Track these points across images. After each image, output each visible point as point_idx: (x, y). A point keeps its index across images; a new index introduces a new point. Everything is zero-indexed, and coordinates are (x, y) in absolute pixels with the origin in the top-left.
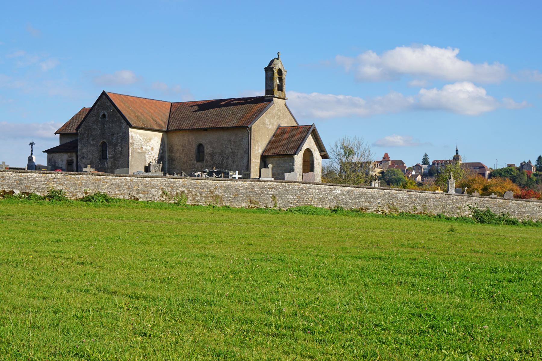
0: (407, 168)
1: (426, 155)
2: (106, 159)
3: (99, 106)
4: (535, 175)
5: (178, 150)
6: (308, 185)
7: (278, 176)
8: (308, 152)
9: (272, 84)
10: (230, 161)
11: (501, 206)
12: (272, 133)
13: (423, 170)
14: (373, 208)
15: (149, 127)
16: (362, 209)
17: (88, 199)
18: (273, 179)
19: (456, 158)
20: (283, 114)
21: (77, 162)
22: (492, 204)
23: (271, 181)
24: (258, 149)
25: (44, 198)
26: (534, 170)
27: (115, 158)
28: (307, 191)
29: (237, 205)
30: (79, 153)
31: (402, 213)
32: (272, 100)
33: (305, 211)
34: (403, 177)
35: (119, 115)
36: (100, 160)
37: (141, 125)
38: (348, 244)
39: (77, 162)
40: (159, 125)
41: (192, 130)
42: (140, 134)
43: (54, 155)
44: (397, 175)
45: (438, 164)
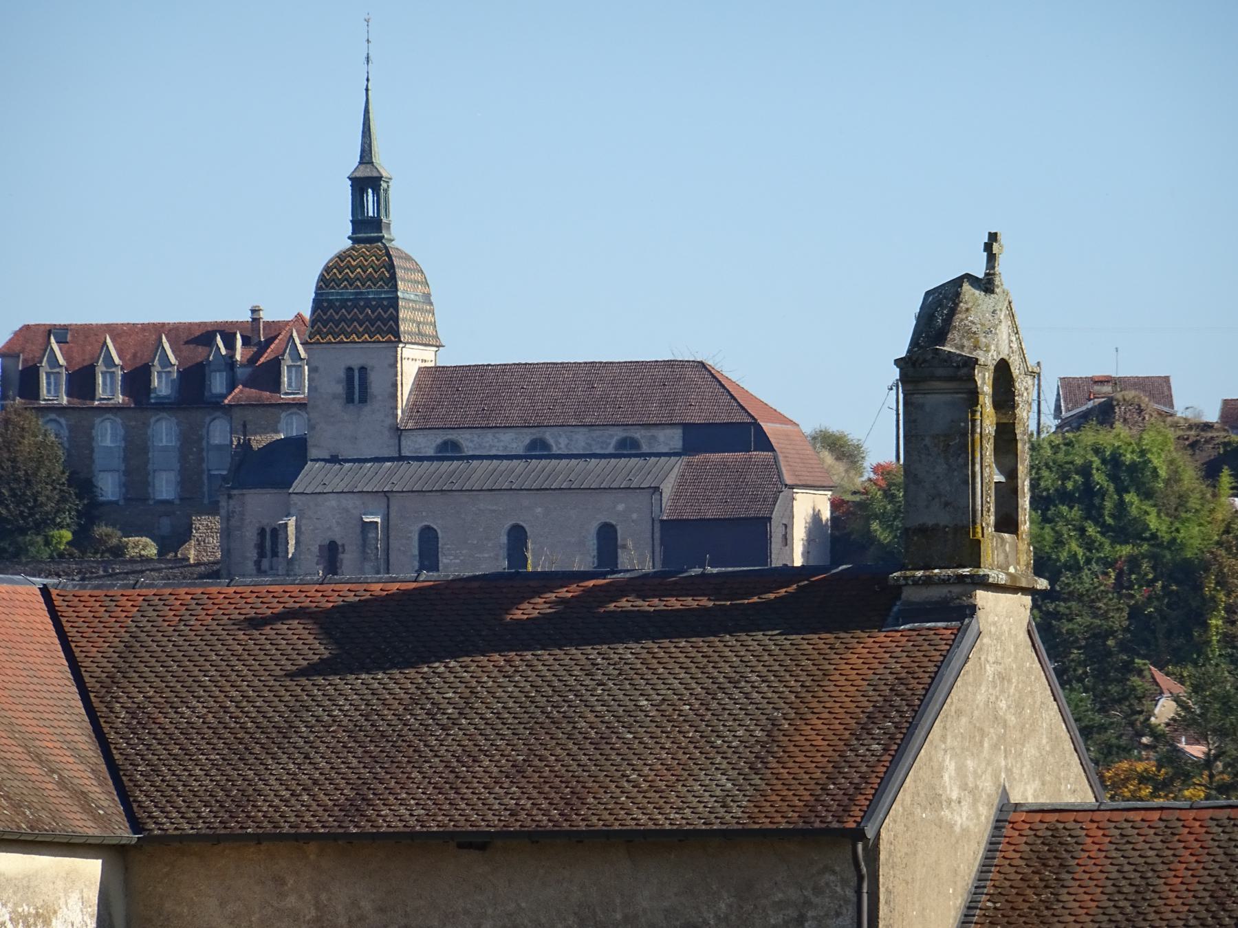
12: (967, 859)
19: (362, 296)
20: (1019, 707)
32: (973, 610)
45: (82, 381)
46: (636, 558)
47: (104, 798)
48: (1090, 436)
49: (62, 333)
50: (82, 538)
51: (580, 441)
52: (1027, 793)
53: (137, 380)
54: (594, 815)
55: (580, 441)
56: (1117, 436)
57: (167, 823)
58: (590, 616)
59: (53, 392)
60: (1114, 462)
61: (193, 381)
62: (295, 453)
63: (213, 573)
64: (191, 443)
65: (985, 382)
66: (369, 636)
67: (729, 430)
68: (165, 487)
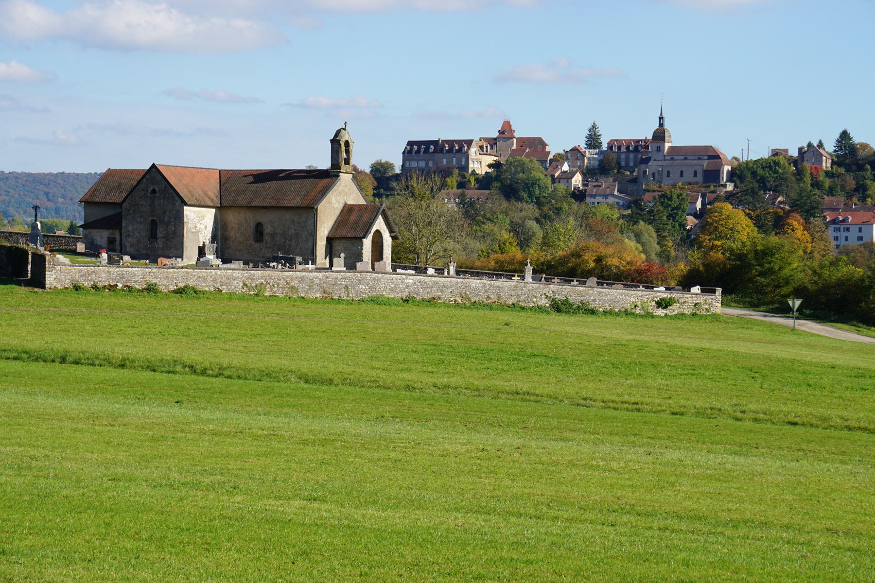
0: (551, 157)
1: (594, 127)
4: (828, 174)
5: (232, 228)
6: (380, 275)
7: (351, 266)
8: (378, 233)
9: (339, 158)
11: (580, 295)
12: (337, 212)
13: (586, 160)
14: (445, 297)
15: (203, 203)
16: (434, 299)
17: (180, 291)
19: (660, 135)
22: (573, 292)
23: (344, 272)
24: (323, 231)
25: (142, 290)
26: (826, 164)
27: (167, 238)
28: (379, 280)
29: (312, 296)
30: (123, 231)
31: (475, 302)
33: (377, 301)
34: (542, 177)
35: (172, 191)
37: (195, 202)
38: (419, 337)
40: (212, 200)
41: (249, 208)
42: (194, 212)
43: (91, 230)
44: (529, 171)
45: (619, 148)
49: (617, 140)
51: (692, 158)
53: (628, 148)
55: (692, 158)
57: (224, 204)
59: (615, 149)
61: (636, 148)
62: (649, 159)
64: (635, 157)
65: (343, 144)
68: (631, 164)
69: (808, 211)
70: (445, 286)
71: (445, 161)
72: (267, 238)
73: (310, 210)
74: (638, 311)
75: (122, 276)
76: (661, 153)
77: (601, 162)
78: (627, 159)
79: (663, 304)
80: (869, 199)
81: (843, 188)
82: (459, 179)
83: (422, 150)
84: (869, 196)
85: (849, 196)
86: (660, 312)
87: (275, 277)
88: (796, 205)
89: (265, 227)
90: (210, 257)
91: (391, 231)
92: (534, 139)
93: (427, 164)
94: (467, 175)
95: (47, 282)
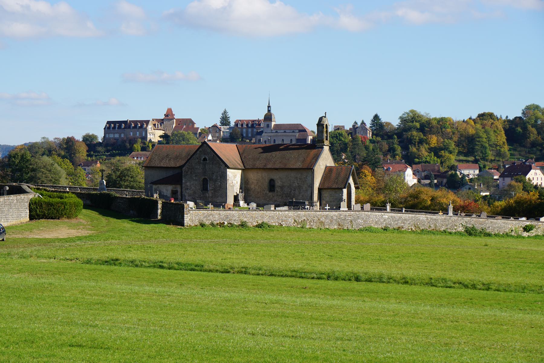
0: (199, 131)
1: (225, 112)
2: (207, 190)
3: (201, 152)
4: (372, 141)
5: (253, 183)
10: (297, 192)
14: (406, 227)
18: (347, 209)
19: (268, 117)
21: (182, 192)
22: (473, 221)
23: (346, 211)
26: (369, 135)
28: (369, 216)
30: (183, 185)
33: (369, 230)
36: (202, 191)
39: (182, 192)
41: (264, 169)
43: (159, 186)
45: (242, 125)
46: (294, 143)
47: (242, 165)
48: (337, 131)
49: (240, 121)
50: (242, 140)
51: (289, 131)
52: (328, 165)
53: (247, 125)
54: (288, 167)
55: (289, 131)
56: (339, 131)
58: (287, 148)
59: (239, 126)
60: (339, 134)
61: (253, 125)
62: (262, 132)
63: (254, 143)
64: (252, 131)
65: (325, 126)
66: (266, 150)
67: (303, 130)
68: (250, 135)
69: (373, 164)
70: (405, 220)
71: (132, 133)
72: (277, 189)
73: (310, 170)
74: (513, 234)
75: (227, 217)
76: (269, 129)
77: (231, 134)
78: (247, 132)
79: (527, 229)
80: (397, 157)
81: (381, 150)
82: (142, 145)
83: (117, 127)
84: (397, 155)
85: (385, 155)
86: (525, 234)
87: (281, 216)
88: (366, 161)
89: (276, 182)
90: (242, 203)
91: (355, 184)
92: (187, 120)
93: (120, 136)
94: (147, 143)
95: (185, 222)
